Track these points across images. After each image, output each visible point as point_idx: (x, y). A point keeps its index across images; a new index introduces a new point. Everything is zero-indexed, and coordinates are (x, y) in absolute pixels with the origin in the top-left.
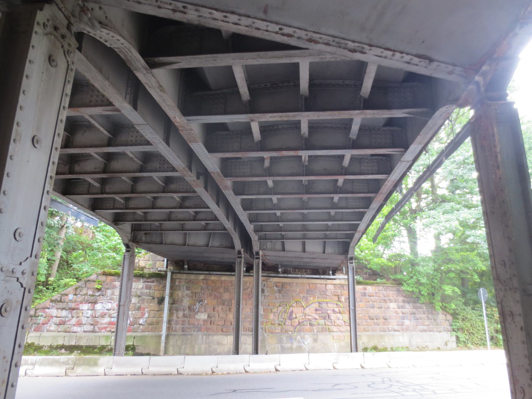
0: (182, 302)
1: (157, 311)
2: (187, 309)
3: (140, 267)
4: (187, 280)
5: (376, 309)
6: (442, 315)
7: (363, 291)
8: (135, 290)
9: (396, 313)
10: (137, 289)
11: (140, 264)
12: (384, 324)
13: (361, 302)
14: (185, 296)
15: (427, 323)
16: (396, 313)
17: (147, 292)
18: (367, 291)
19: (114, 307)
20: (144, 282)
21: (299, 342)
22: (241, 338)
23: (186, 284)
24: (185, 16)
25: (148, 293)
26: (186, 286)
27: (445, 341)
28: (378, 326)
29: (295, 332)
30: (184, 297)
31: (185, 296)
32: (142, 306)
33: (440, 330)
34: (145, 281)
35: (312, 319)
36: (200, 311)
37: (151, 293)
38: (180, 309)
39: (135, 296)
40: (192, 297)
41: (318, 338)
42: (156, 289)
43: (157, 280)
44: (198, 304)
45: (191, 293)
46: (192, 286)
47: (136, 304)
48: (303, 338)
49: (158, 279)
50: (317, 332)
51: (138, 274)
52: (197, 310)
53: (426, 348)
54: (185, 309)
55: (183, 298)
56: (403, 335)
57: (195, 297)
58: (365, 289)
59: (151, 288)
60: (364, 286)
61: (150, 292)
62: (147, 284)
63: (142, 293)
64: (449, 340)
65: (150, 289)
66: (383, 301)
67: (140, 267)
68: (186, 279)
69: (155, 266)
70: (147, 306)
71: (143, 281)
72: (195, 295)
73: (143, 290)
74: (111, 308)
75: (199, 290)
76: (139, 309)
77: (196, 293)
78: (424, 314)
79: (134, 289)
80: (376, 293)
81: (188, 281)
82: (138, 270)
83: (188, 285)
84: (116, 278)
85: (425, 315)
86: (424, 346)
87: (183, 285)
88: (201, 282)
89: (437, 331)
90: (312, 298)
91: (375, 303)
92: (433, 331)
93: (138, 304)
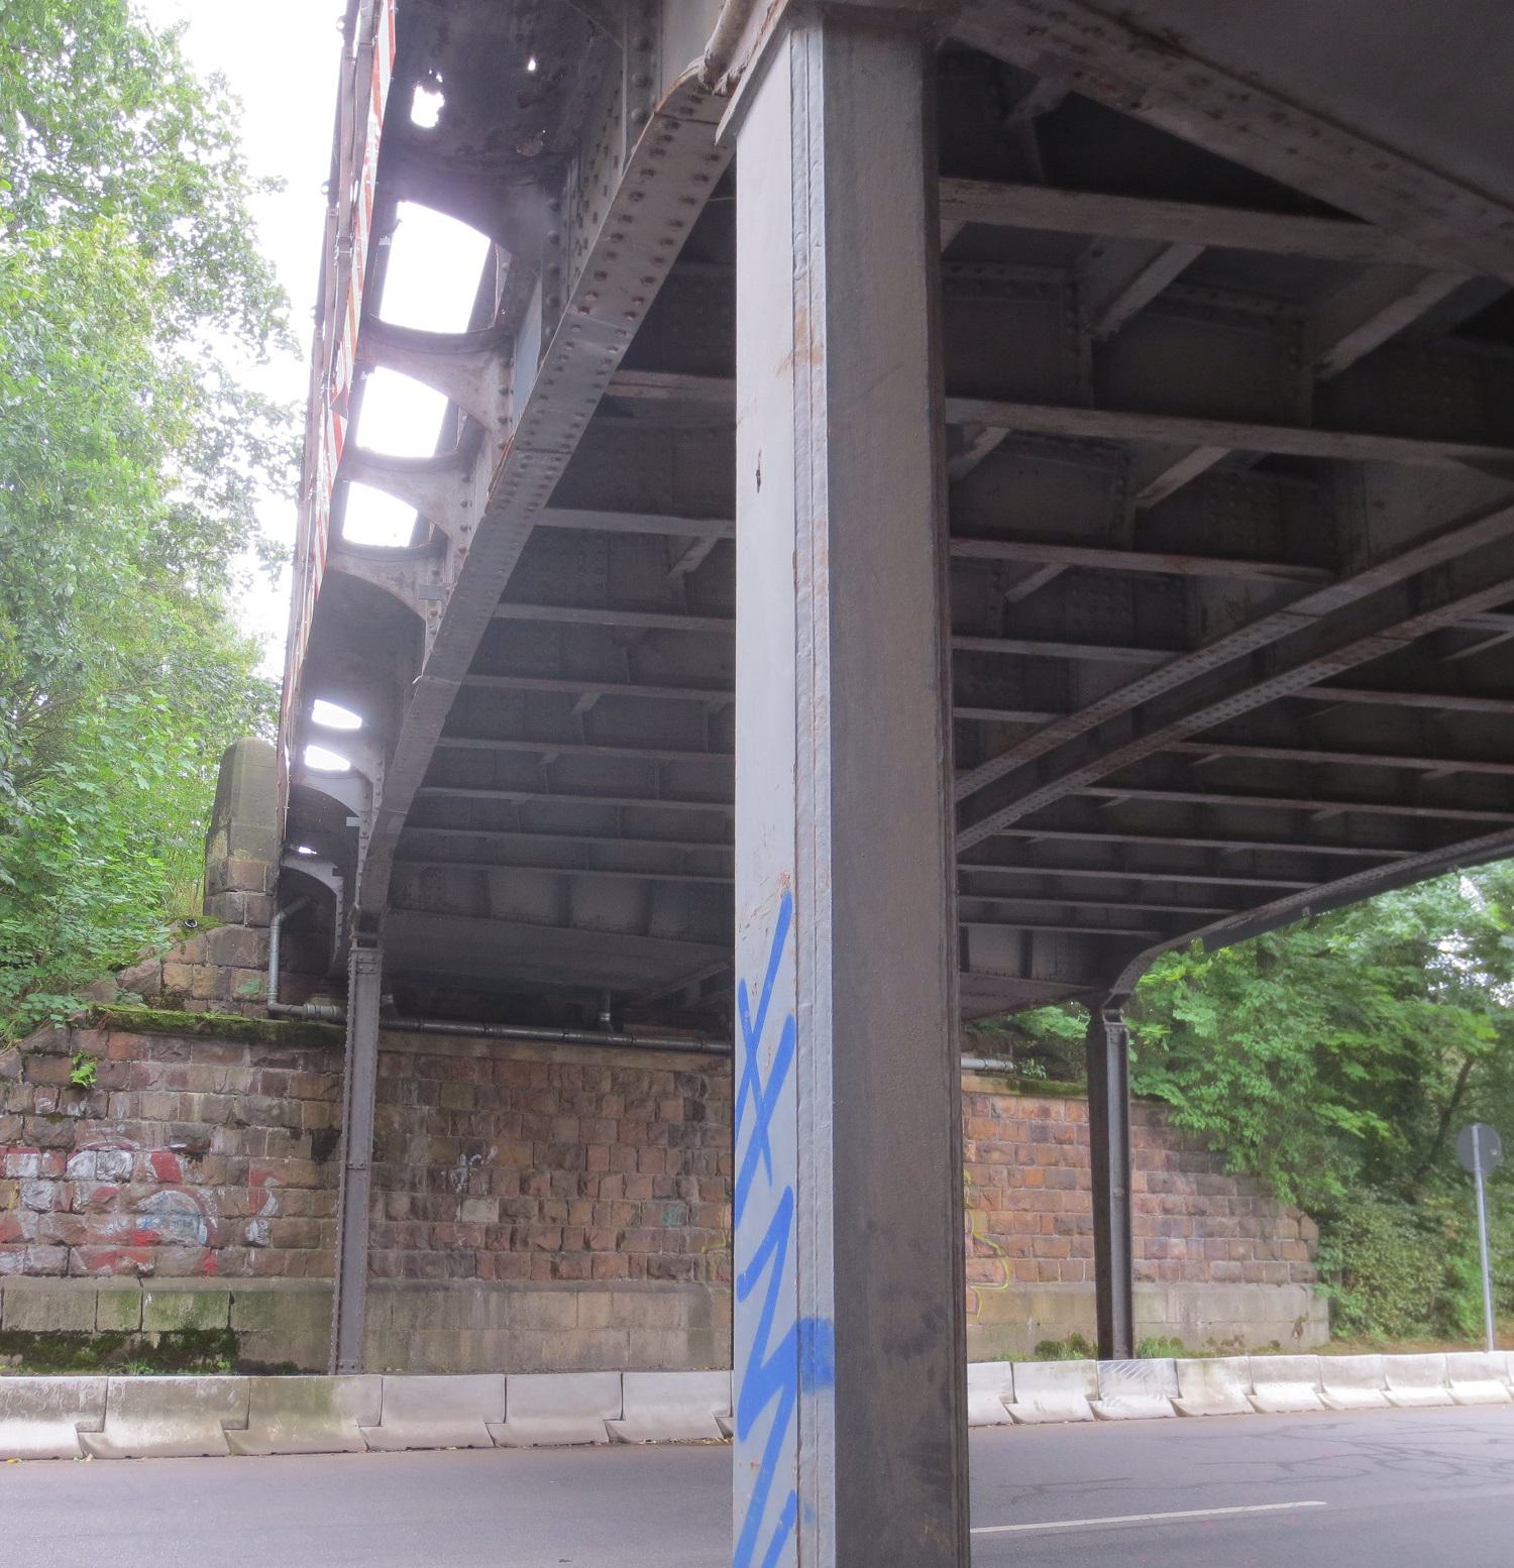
0: (404, 1149)
1: (310, 1188)
3: (167, 991)
4: (423, 1060)
10: (230, 1092)
14: (416, 1127)
17: (270, 1108)
18: (1050, 1122)
19: (143, 1169)
20: (256, 1064)
25: (275, 1112)
26: (420, 1085)
27: (1296, 1317)
30: (411, 1132)
31: (416, 1127)
32: (252, 1166)
36: (472, 1191)
37: (287, 1110)
38: (401, 1180)
39: (224, 1125)
40: (442, 1131)
42: (303, 1096)
45: (440, 1112)
46: (441, 1084)
51: (235, 1027)
55: (408, 1135)
59: (285, 1089)
61: (281, 1107)
62: (271, 1070)
63: (248, 1110)
64: (1307, 1314)
65: (281, 1096)
67: (167, 991)
68: (417, 1056)
69: (228, 990)
71: (255, 1060)
72: (455, 1124)
73: (252, 1097)
74: (131, 1173)
75: (469, 1106)
77: (455, 1114)
78: (1232, 1213)
82: (162, 1007)
86: (1231, 1338)
93: (236, 1159)
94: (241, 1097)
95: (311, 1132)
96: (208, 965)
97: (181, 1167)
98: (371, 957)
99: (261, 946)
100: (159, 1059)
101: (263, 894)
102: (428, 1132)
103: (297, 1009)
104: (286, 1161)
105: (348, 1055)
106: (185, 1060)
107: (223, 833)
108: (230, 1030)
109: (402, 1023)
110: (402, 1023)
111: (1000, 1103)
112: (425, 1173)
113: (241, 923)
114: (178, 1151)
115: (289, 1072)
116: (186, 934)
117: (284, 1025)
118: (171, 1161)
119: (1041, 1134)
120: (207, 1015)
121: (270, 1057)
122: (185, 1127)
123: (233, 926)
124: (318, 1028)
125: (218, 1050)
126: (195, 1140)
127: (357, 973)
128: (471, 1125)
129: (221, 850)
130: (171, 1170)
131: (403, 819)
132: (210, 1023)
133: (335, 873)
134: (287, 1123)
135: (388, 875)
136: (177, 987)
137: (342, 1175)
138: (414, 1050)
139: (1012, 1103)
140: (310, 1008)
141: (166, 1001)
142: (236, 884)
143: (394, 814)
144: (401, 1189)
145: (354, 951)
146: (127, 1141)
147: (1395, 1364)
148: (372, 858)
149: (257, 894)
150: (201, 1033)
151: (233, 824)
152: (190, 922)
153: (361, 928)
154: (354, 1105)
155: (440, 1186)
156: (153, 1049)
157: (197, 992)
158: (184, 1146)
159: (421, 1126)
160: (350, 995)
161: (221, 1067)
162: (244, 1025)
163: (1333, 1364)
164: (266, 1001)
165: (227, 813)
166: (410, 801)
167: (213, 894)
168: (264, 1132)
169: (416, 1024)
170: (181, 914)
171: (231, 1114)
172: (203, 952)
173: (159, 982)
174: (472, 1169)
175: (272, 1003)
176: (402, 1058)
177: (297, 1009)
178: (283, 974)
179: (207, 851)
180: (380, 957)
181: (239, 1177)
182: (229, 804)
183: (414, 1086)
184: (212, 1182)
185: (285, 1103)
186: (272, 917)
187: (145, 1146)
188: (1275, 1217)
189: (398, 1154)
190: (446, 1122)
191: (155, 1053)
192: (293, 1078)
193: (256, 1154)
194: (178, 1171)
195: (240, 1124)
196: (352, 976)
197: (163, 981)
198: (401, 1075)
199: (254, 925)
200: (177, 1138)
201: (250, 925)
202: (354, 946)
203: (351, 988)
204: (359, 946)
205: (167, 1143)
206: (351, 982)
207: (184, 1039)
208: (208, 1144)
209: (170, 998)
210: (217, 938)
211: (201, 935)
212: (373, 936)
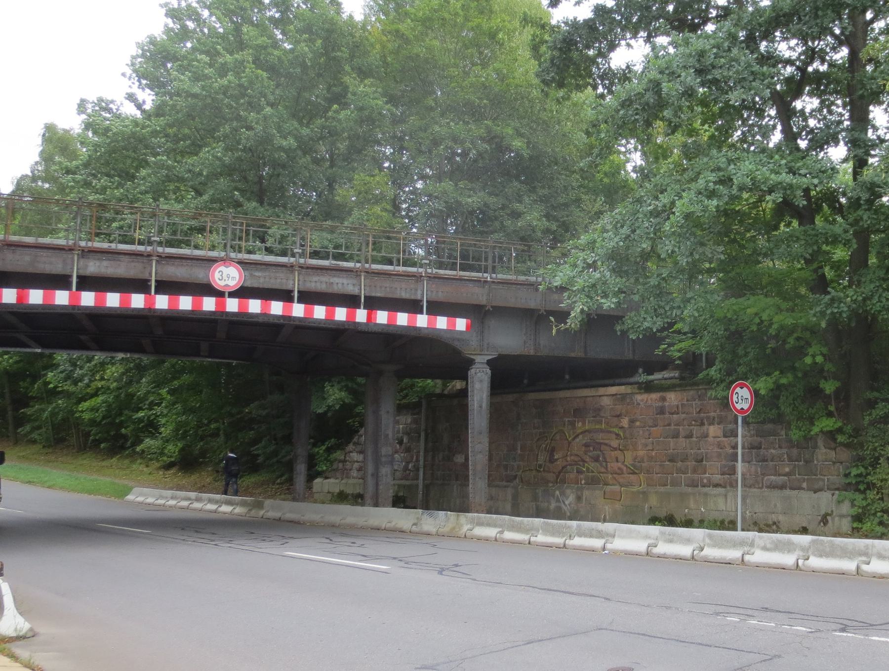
5: (681, 440)
6: (824, 451)
7: (660, 404)
9: (720, 446)
12: (695, 471)
13: (656, 426)
15: (787, 470)
16: (720, 446)
18: (667, 404)
21: (558, 501)
22: (42, 484)
24: (135, 90)
27: (823, 512)
28: (683, 476)
29: (557, 483)
33: (816, 487)
35: (579, 461)
41: (582, 494)
48: (563, 493)
50: (585, 484)
53: (774, 527)
56: (726, 496)
58: (663, 399)
60: (661, 394)
64: (832, 511)
66: (693, 423)
78: (780, 447)
80: (682, 405)
85: (785, 451)
86: (771, 523)
89: (809, 489)
90: (580, 424)
91: (681, 428)
92: (800, 488)
111: (639, 397)
119: (661, 411)
139: (645, 396)
147: (547, 524)
163: (513, 521)
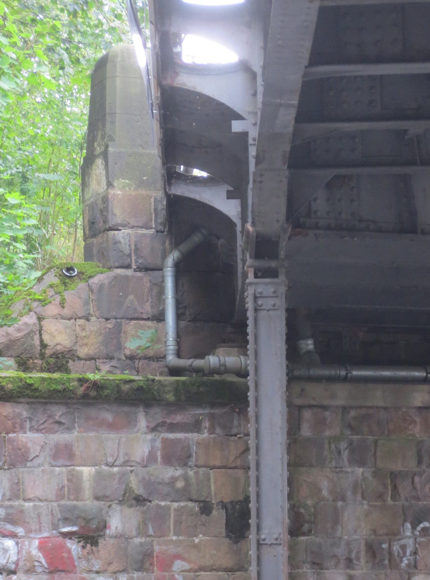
0: (336, 521)
1: (226, 570)
2: (363, 554)
3: (48, 352)
4: (353, 413)
8: (115, 469)
10: (125, 463)
11: (46, 338)
14: (349, 494)
17: (173, 480)
19: (30, 558)
20: (153, 430)
23: (348, 432)
25: (180, 484)
26: (351, 443)
30: (343, 499)
31: (349, 494)
32: (157, 548)
34: (163, 424)
36: (420, 565)
37: (193, 480)
38: (335, 556)
39: (121, 502)
40: (381, 496)
42: (212, 463)
43: (212, 417)
44: (408, 533)
45: (376, 474)
46: (376, 442)
47: (128, 539)
49: (217, 411)
51: (125, 388)
52: (405, 561)
54: (353, 555)
55: (340, 504)
57: (393, 498)
59: (190, 456)
61: (186, 478)
62: (171, 436)
63: (147, 484)
65: (185, 465)
67: (48, 352)
68: (345, 409)
69: (120, 347)
70: (180, 550)
71: (153, 425)
72: (395, 488)
73: (151, 468)
74: (17, 564)
75: (411, 464)
76: (147, 565)
77: (394, 476)
79: (113, 465)
81: (354, 418)
82: (42, 370)
83: (356, 437)
84: (25, 414)
87: (336, 439)
88: (414, 422)
93: (138, 540)
94: (139, 469)
95: (224, 505)
96: (93, 319)
97: (74, 553)
98: (272, 290)
99: (155, 292)
100: (38, 431)
101: (152, 231)
102: (363, 498)
103: (198, 363)
104: (197, 540)
105: (251, 410)
106: (70, 429)
107: (99, 162)
108: (119, 391)
109: (326, 372)
110: (326, 372)
112: (363, 548)
113: (128, 267)
114: (69, 535)
115: (193, 437)
116: (65, 284)
117: (184, 382)
118: (62, 547)
120: (91, 376)
121: (168, 421)
122: (75, 507)
123: (119, 271)
124: (223, 383)
125: (109, 417)
126: (88, 521)
127: (256, 310)
128: (415, 488)
129: (99, 183)
130: (62, 558)
131: (293, 112)
132: (96, 385)
133: (230, 196)
134: (195, 497)
135: (284, 187)
136: (59, 348)
137: (253, 553)
138: (340, 402)
140: (212, 360)
141: (48, 364)
142: (119, 221)
143: (281, 105)
144: (336, 566)
145: (251, 284)
146: (9, 527)
148: (260, 167)
149: (145, 231)
150: (85, 396)
151: (111, 149)
152: (69, 269)
153: (258, 255)
154: (263, 467)
155: (383, 560)
156: (31, 420)
157: (82, 352)
158: (75, 529)
159: (355, 493)
160: (250, 338)
161: (113, 436)
162: (135, 385)
164: (164, 357)
165: (103, 138)
166: (298, 87)
167: (94, 236)
168: (168, 508)
169: (343, 373)
170: (57, 262)
171: (128, 490)
172: (87, 303)
173: (37, 342)
174: (420, 539)
175: (171, 359)
176: (327, 413)
177: (198, 363)
178: (183, 324)
179: (84, 185)
180: (282, 290)
181: (142, 562)
182: (104, 126)
183: (343, 445)
184: (112, 568)
185: (191, 473)
186: (164, 257)
187: (30, 531)
188: (159, 553)
189: (329, 525)
190: (385, 486)
191: (34, 424)
192: (198, 444)
193: (161, 533)
194: (71, 558)
195: (140, 501)
196: (250, 314)
197: (42, 341)
198: (327, 433)
199: (146, 269)
200: (66, 520)
201: (139, 269)
202: (251, 278)
203: (250, 329)
204: (256, 276)
205: (55, 527)
206: (250, 322)
207: (66, 404)
208: (105, 526)
209: (52, 360)
210: (101, 287)
211: (82, 285)
212: (273, 264)
